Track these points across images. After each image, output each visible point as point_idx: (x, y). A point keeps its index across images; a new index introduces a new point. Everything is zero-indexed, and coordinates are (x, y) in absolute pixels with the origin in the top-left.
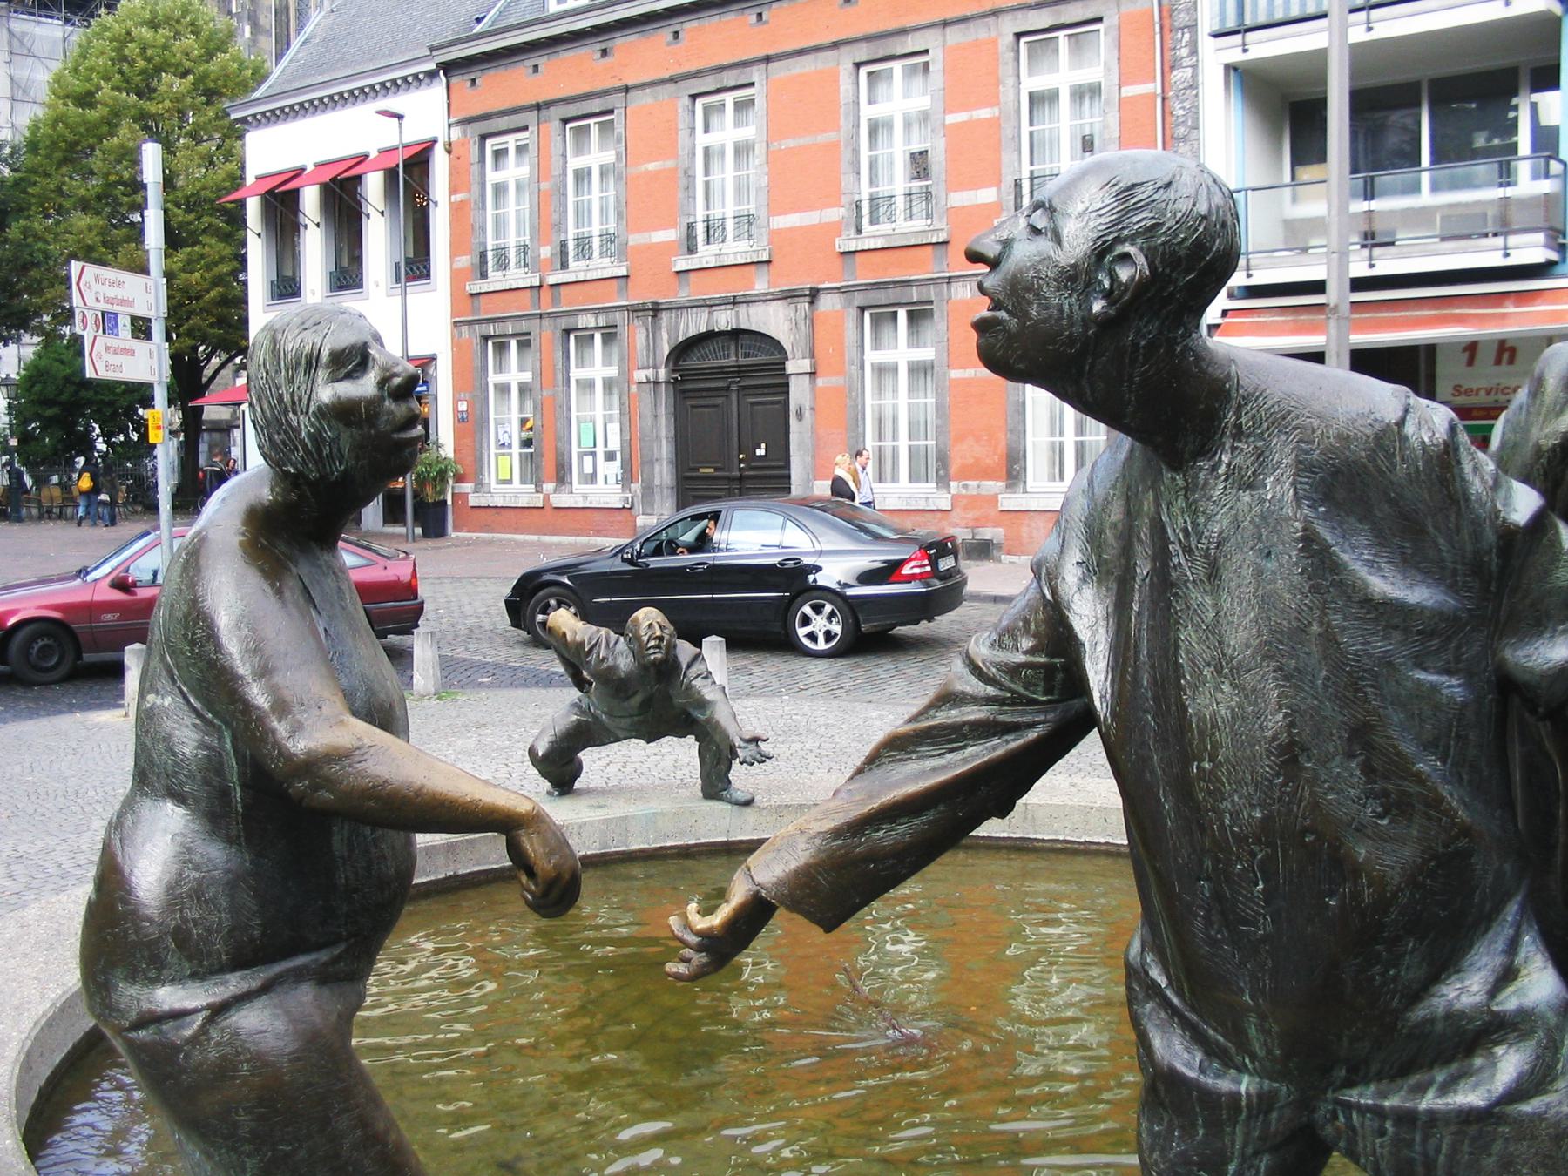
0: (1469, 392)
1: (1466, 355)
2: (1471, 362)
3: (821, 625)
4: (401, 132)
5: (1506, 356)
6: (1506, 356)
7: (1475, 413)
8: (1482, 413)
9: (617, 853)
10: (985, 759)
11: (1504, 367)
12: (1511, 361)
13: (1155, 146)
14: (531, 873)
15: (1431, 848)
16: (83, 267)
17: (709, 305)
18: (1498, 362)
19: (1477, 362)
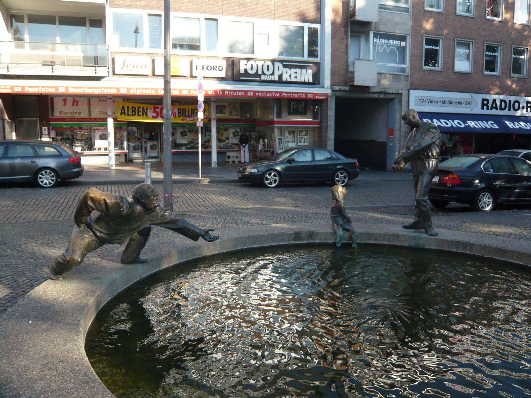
0: (65, 113)
1: (63, 102)
2: (65, 104)
3: (46, 180)
4: (268, 40)
5: (75, 103)
6: (75, 103)
7: (67, 120)
8: (94, 120)
9: (144, 278)
10: (213, 253)
11: (75, 106)
12: (77, 105)
13: (437, 50)
14: (228, 303)
15: (503, 354)
16: (172, 76)
17: (95, 88)
18: (73, 105)
19: (67, 104)
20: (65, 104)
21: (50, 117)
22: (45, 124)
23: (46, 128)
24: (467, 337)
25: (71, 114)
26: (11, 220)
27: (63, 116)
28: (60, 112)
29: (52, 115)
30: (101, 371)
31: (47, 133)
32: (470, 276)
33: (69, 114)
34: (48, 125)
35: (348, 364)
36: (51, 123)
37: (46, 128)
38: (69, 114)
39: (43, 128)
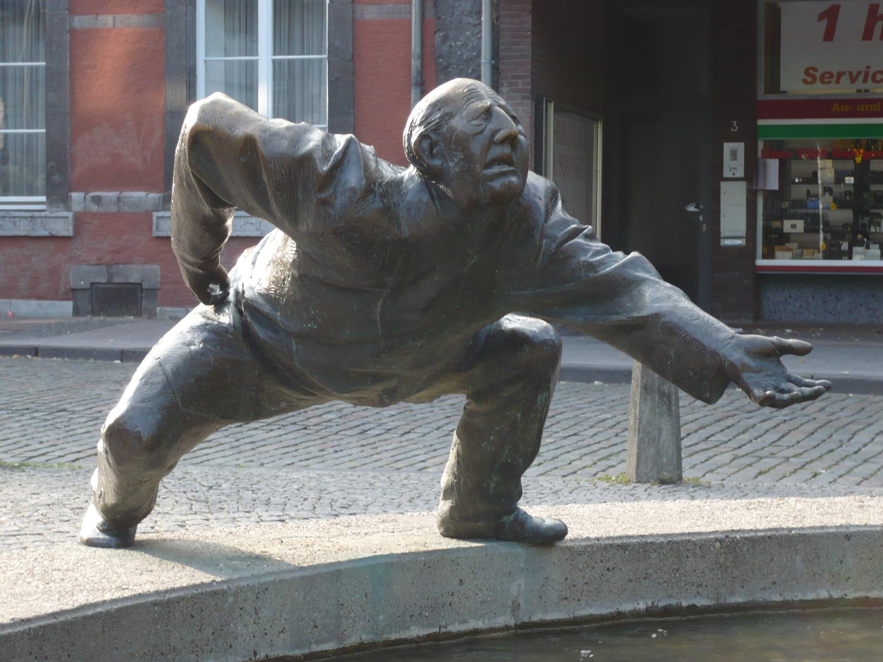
1: (824, 23)
2: (829, 35)
7: (836, 108)
20: (829, 35)
21: (762, 95)
22: (735, 126)
23: (740, 147)
24: (303, 474)
25: (853, 80)
26: (57, 422)
27: (819, 90)
28: (807, 72)
29: (774, 85)
30: (348, 265)
31: (740, 173)
32: (481, 547)
33: (845, 79)
34: (749, 136)
35: (587, 608)
36: (761, 122)
37: (740, 147)
38: (845, 79)
39: (728, 147)
